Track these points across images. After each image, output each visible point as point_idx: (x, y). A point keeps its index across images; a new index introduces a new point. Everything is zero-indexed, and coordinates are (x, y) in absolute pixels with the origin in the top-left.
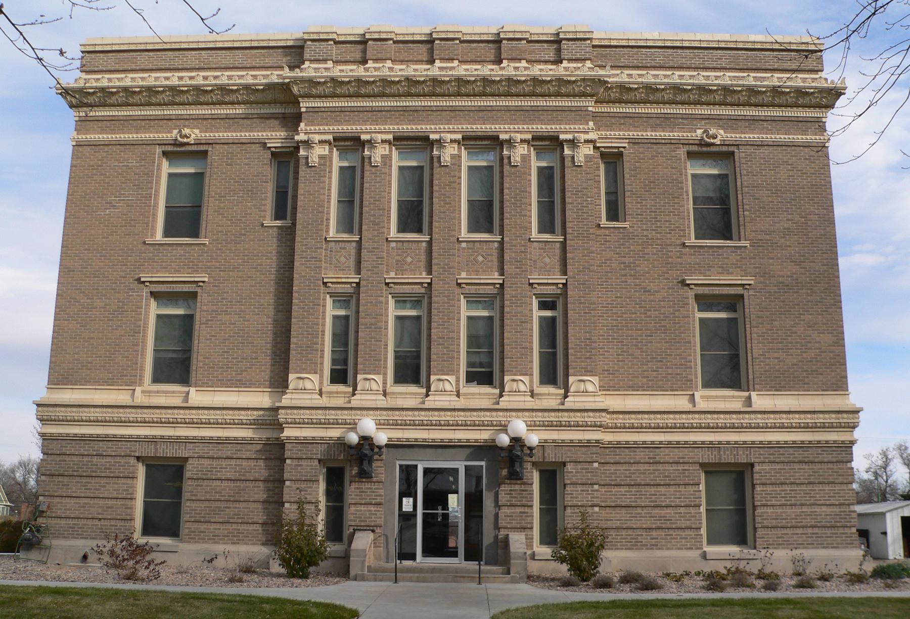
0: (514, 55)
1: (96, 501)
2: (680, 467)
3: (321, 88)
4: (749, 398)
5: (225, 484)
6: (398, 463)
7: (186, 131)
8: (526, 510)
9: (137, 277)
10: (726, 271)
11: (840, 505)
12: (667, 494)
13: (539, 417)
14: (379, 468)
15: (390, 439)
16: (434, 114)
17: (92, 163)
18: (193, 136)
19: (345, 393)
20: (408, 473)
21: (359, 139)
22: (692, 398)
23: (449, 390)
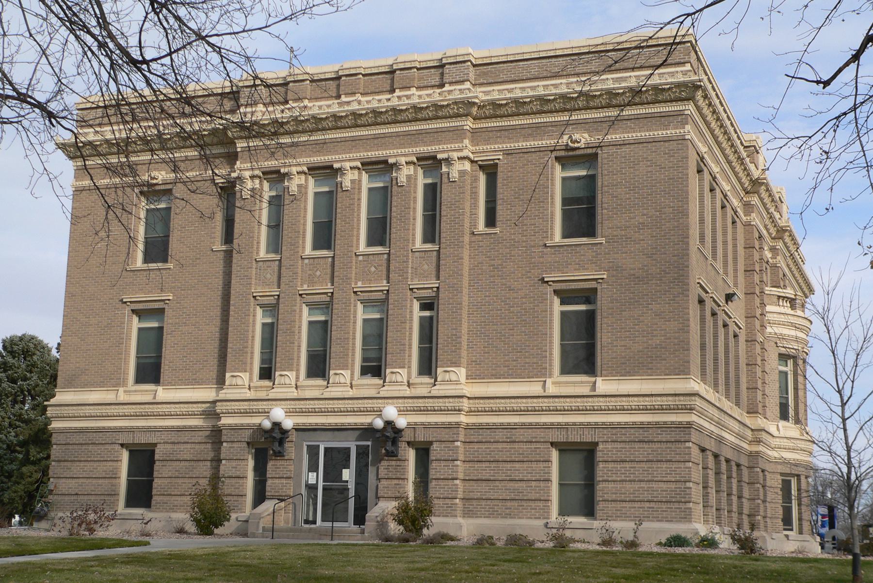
0: (405, 84)
2: (533, 446)
5: (183, 463)
6: (305, 443)
7: (576, 136)
8: (401, 482)
10: (582, 267)
12: (521, 470)
13: (410, 403)
14: (290, 448)
15: (409, 424)
16: (339, 144)
18: (583, 140)
19: (428, 384)
20: (313, 451)
21: (331, 167)
23: (346, 380)
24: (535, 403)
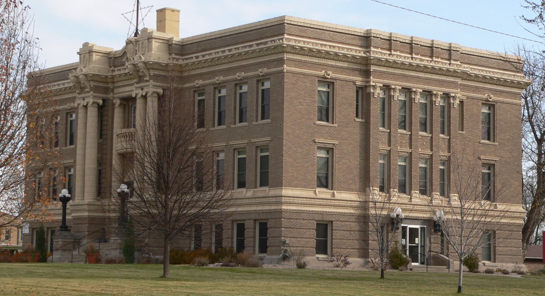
1: (303, 239)
4: (334, 193)
11: (340, 239)
24: (313, 201)
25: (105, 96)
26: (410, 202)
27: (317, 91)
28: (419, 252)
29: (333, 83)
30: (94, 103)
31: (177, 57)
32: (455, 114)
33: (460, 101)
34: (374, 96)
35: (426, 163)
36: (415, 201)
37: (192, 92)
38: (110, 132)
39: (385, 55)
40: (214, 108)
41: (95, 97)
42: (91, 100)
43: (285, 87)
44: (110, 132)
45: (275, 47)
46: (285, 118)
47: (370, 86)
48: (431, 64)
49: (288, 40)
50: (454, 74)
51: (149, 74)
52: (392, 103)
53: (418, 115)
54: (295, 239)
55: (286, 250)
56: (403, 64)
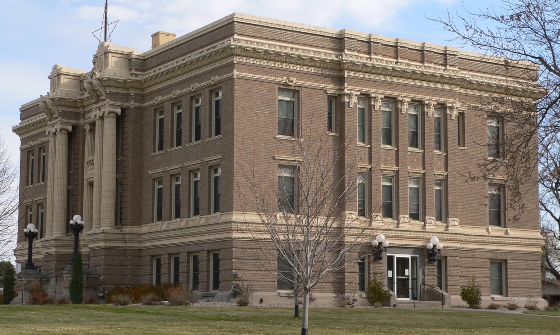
3: (356, 67)
4: (507, 231)
7: (291, 79)
9: (272, 156)
15: (389, 244)
17: (245, 89)
22: (487, 230)
25: (75, 122)
26: (397, 227)
27: (277, 100)
28: (410, 287)
29: (298, 91)
30: (61, 130)
31: (136, 72)
32: (452, 127)
33: (458, 113)
34: (349, 105)
35: (417, 183)
36: (402, 226)
37: (153, 111)
38: (81, 161)
39: (361, 59)
40: (172, 126)
41: (64, 123)
42: (59, 127)
43: (236, 95)
44: (81, 161)
45: (224, 50)
46: (235, 131)
47: (344, 94)
48: (420, 69)
49: (238, 41)
50: (451, 81)
51: (106, 92)
52: (373, 114)
53: (405, 129)
54: (250, 272)
55: (237, 285)
56: (384, 68)
